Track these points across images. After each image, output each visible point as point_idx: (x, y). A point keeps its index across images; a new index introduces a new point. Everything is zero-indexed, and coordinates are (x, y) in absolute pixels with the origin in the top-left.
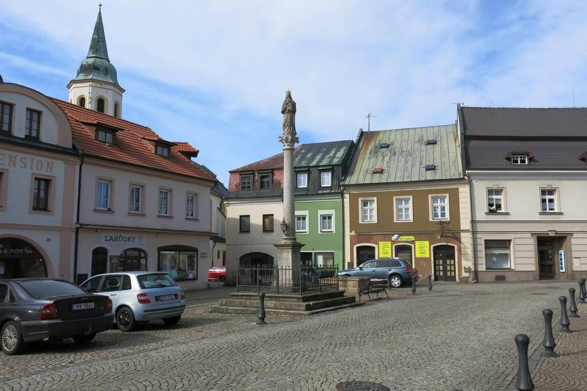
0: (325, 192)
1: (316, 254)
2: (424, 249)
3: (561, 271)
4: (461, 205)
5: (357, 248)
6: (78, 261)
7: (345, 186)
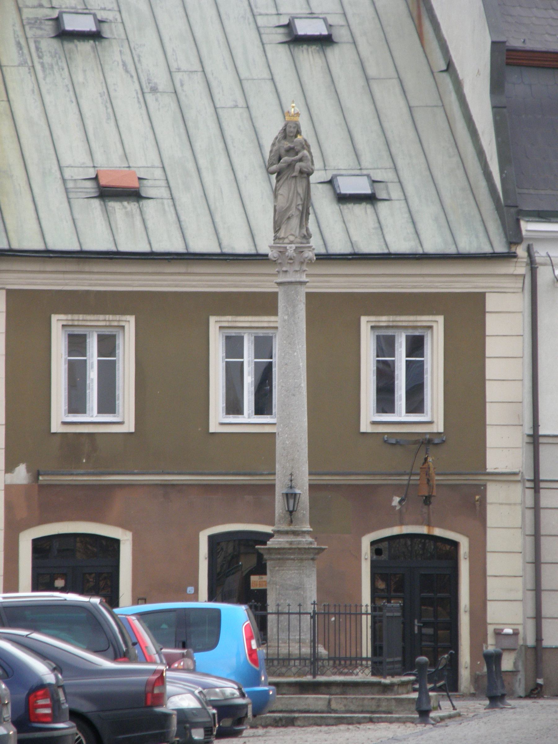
4: (492, 369)
6: (540, 423)
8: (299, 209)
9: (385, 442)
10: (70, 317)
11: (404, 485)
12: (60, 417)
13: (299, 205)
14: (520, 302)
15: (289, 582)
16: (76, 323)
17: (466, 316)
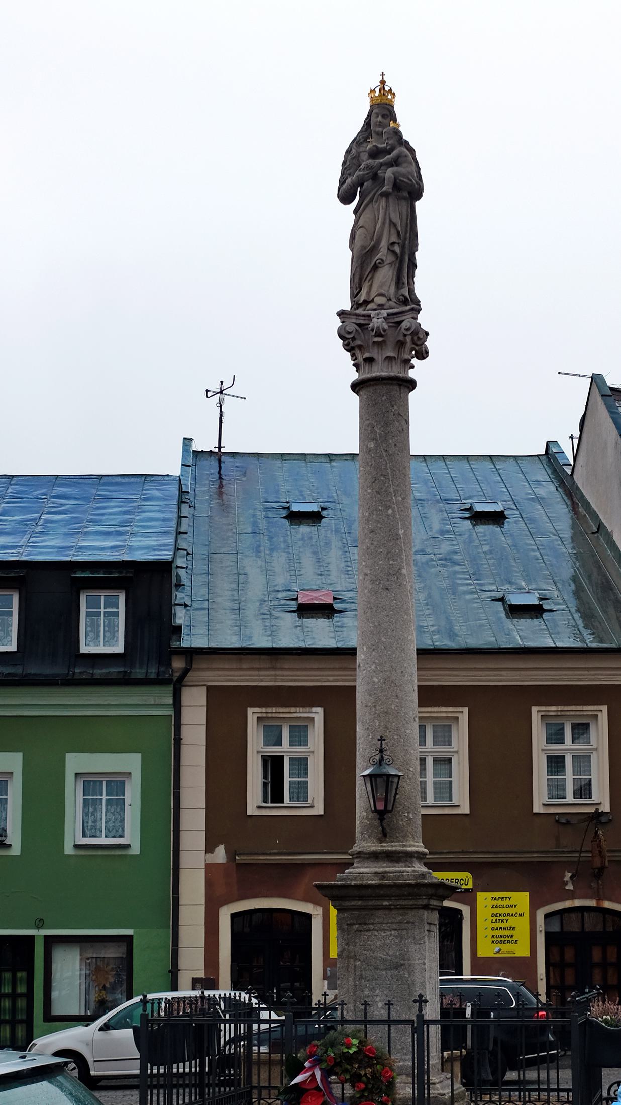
1: (51, 942)
2: (512, 922)
5: (234, 916)
7: (192, 654)
8: (394, 252)
9: (557, 821)
10: (264, 710)
11: (574, 862)
12: (255, 801)
13: (393, 244)
15: (380, 955)
16: (270, 715)
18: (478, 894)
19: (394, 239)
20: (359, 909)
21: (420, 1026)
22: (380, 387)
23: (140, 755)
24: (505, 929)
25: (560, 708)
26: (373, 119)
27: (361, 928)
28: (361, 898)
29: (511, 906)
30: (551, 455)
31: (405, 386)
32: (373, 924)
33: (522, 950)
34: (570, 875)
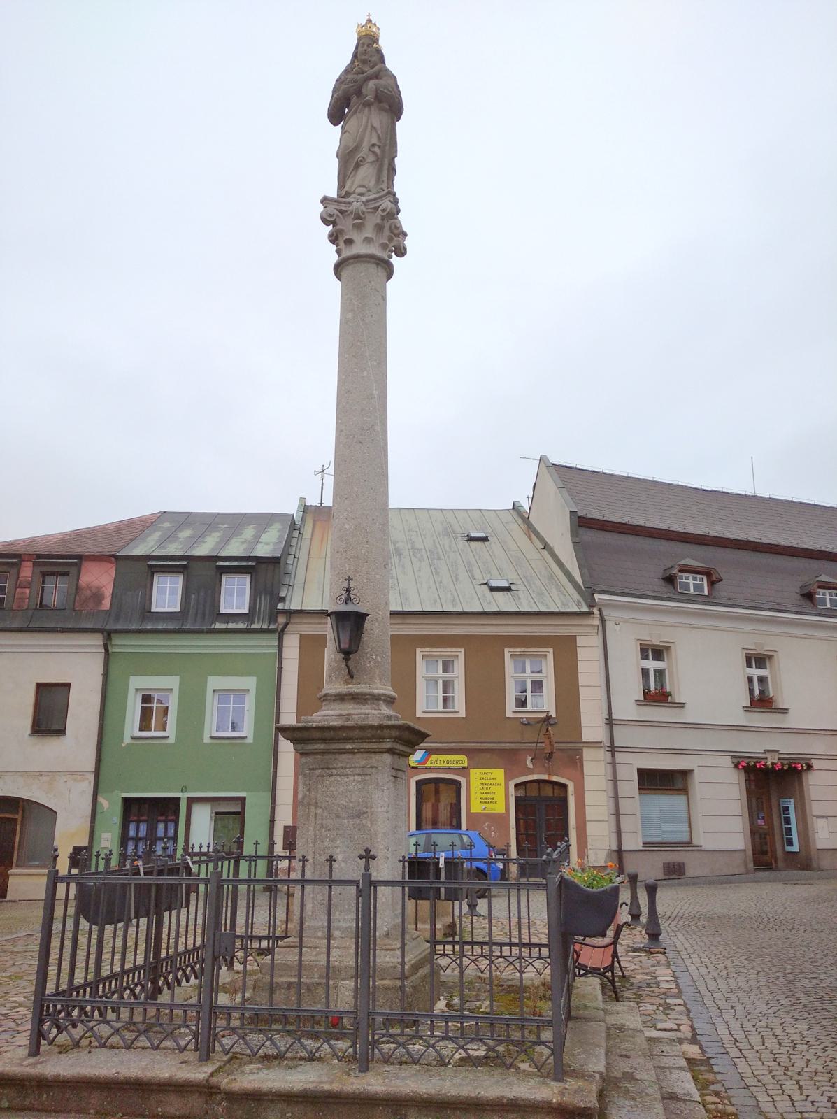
0: (231, 626)
1: (191, 801)
2: (493, 789)
3: (789, 849)
4: (582, 680)
5: (418, 782)
6: (613, 711)
7: (289, 613)
8: (374, 152)
13: (374, 145)
14: (597, 641)
17: (566, 649)
18: (471, 770)
19: (374, 141)
20: (323, 752)
21: (367, 887)
22: (359, 265)
23: (255, 678)
24: (489, 793)
25: (523, 650)
26: (360, 49)
27: (323, 773)
28: (324, 740)
29: (493, 779)
30: (515, 507)
31: (383, 267)
32: (335, 768)
33: (499, 808)
34: (531, 758)
